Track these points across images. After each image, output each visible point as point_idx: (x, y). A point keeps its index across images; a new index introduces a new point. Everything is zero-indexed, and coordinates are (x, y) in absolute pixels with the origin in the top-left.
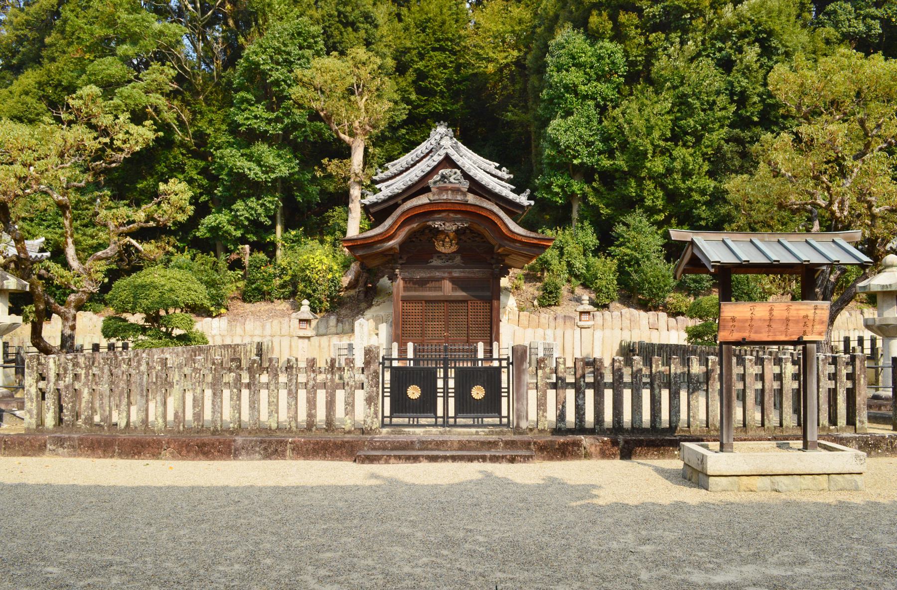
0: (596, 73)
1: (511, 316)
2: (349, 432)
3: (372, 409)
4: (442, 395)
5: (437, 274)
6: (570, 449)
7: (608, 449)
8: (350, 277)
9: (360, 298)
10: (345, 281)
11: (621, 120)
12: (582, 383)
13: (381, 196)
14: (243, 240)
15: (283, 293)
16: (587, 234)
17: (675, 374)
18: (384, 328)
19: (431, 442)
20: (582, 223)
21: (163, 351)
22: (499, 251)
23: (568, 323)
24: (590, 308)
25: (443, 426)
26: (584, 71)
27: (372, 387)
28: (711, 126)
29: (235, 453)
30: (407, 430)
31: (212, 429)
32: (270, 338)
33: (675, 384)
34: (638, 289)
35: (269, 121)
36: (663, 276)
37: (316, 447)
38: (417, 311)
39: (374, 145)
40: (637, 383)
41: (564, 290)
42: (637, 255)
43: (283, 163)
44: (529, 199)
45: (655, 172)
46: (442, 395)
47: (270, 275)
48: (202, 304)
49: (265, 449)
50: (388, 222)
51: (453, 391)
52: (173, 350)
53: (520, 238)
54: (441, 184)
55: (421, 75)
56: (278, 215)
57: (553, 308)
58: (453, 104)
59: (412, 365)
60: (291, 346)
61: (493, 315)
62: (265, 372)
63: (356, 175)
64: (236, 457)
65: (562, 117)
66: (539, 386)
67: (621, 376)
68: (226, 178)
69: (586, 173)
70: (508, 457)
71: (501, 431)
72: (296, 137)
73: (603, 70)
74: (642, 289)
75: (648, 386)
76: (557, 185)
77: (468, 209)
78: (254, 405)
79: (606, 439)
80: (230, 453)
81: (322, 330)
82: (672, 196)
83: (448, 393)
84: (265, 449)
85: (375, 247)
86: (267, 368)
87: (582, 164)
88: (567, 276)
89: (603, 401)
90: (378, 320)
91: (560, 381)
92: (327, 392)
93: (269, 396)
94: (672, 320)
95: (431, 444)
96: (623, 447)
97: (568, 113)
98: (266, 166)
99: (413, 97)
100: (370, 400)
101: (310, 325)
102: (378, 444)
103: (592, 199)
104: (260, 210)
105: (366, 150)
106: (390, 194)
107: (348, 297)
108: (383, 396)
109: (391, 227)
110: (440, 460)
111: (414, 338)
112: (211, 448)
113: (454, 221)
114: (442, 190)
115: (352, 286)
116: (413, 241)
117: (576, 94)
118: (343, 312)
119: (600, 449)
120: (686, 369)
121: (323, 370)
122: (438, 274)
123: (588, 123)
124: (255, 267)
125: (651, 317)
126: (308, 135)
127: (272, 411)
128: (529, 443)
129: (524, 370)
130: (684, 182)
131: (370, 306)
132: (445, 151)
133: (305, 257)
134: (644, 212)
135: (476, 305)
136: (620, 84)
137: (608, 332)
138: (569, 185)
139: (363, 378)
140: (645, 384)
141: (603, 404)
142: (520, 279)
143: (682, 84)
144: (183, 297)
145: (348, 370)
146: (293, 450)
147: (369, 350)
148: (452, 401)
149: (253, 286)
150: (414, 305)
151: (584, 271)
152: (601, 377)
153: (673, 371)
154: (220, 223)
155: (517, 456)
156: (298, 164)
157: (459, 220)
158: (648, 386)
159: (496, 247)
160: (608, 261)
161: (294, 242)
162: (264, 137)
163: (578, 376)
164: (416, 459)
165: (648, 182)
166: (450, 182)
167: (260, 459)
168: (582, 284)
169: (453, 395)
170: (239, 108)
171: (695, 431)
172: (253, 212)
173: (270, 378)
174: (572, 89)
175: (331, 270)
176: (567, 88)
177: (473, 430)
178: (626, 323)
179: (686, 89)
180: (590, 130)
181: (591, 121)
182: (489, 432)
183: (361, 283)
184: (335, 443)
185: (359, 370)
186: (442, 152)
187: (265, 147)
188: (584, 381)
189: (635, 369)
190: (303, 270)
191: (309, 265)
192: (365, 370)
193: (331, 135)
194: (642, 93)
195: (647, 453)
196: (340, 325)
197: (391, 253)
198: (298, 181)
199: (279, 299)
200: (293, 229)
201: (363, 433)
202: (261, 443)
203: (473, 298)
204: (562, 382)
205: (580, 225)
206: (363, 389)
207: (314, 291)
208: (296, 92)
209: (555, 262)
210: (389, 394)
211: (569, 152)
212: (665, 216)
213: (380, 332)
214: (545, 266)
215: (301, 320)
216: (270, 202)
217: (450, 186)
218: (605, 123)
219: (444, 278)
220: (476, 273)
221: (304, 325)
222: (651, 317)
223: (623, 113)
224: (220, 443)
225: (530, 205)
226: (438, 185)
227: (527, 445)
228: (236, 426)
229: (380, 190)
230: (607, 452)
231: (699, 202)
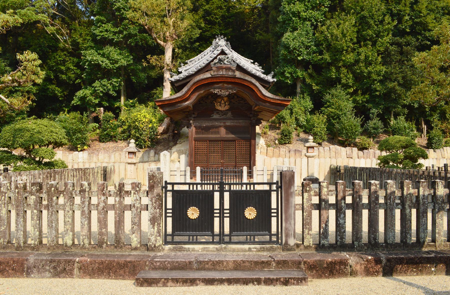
0: (311, 5)
1: (262, 150)
2: (136, 249)
3: (156, 229)
4: (218, 215)
5: (217, 123)
6: (338, 267)
7: (372, 267)
8: (164, 127)
9: (169, 139)
10: (161, 129)
11: (326, 33)
12: (343, 204)
13: (181, 76)
14: (100, 105)
15: (123, 136)
16: (306, 101)
17: (424, 196)
18: (183, 158)
19: (207, 263)
20: (303, 95)
21: (19, 174)
22: (256, 108)
23: (297, 154)
24: (314, 144)
25: (219, 243)
26: (304, 4)
27: (155, 208)
28: (382, 34)
29: (27, 271)
30: (187, 246)
31: (16, 245)
32: (113, 164)
33: (423, 204)
34: (339, 134)
35: (115, 33)
36: (355, 126)
37: (101, 266)
39: (179, 48)
40: (390, 204)
41: (294, 135)
42: (338, 112)
43: (123, 58)
44: (273, 78)
45: (348, 62)
47: (115, 125)
48: (61, 142)
49: (54, 268)
50: (185, 90)
52: (30, 173)
53: (269, 100)
54: (219, 65)
55: (207, 13)
56: (122, 91)
57: (287, 145)
58: (226, 30)
60: (125, 169)
61: (252, 149)
62: (62, 195)
63: (168, 65)
64: (28, 275)
65: (291, 32)
66: (305, 207)
67: (377, 198)
68: (87, 67)
69: (305, 65)
70: (282, 280)
71: (272, 248)
72: (131, 43)
73: (316, 3)
74: (342, 133)
75: (399, 206)
76: (288, 72)
77: (236, 81)
78: (53, 224)
79: (370, 258)
80: (23, 271)
81: (146, 159)
82: (358, 78)
83: (224, 213)
84: (54, 268)
85: (177, 106)
86: (63, 191)
87: (303, 60)
88: (295, 126)
89: (362, 220)
90: (180, 153)
91: (323, 203)
92: (116, 213)
93: (65, 216)
94: (361, 153)
95: (208, 264)
96: (386, 265)
97: (295, 29)
98: (113, 60)
99: (203, 25)
100: (153, 221)
101: (135, 155)
102: (158, 264)
103: (308, 81)
104: (110, 87)
105: (173, 50)
106: (187, 75)
107: (163, 139)
108: (166, 217)
109: (187, 92)
110: (216, 283)
111: (202, 164)
112: (6, 266)
113: (227, 89)
114: (219, 69)
115: (164, 132)
116: (201, 103)
117: (300, 18)
118: (159, 148)
119: (365, 267)
120: (432, 191)
121: (112, 193)
122: (217, 124)
123: (307, 35)
124: (106, 120)
125: (348, 150)
126: (138, 42)
127: (68, 230)
128: (300, 263)
129: (291, 193)
130: (367, 68)
131: (175, 144)
132: (221, 48)
133: (135, 114)
134: (342, 87)
135: (241, 143)
136: (325, 12)
137: (322, 160)
138: (295, 72)
139: (145, 201)
140: (397, 204)
141: (362, 223)
142: (267, 128)
143: (362, 10)
144: (46, 137)
145: (134, 194)
146: (80, 269)
147: (153, 175)
149: (105, 133)
150: (202, 143)
151: (305, 123)
152: (360, 199)
153: (421, 193)
154: (85, 94)
155: (291, 278)
156: (132, 59)
157: (230, 89)
158: (399, 206)
159: (253, 107)
160: (321, 116)
161: (131, 107)
162: (111, 42)
163: (339, 198)
164: (192, 282)
165: (343, 69)
166: (225, 64)
167: (50, 277)
168: (304, 131)
170: (96, 26)
171: (440, 245)
172: (105, 88)
173: (66, 200)
174: (297, 14)
175: (151, 122)
176: (294, 14)
177: (246, 247)
178: (333, 154)
179: (365, 13)
180: (308, 39)
181: (308, 34)
182: (261, 248)
183: (170, 131)
184: (118, 263)
185: (144, 194)
186: (220, 49)
187: (111, 49)
189: (389, 191)
190: (134, 122)
191: (138, 119)
192: (149, 194)
193: (153, 42)
194: (339, 16)
195: (407, 270)
196: (157, 155)
197: (188, 110)
198: (133, 70)
199: (121, 140)
200: (131, 99)
201: (148, 250)
202: (51, 262)
203: (239, 139)
204: (325, 204)
205: (302, 96)
206: (147, 210)
207: (141, 135)
208: (130, 14)
209: (288, 117)
210: (171, 215)
211: (296, 52)
212: (354, 90)
213: (181, 160)
214: (282, 120)
215: (129, 153)
216: (115, 82)
217: (224, 66)
218: (317, 35)
219: (220, 126)
220: (241, 123)
221: (131, 156)
222: (348, 150)
223: (328, 29)
224: (14, 261)
225: (274, 81)
226: (217, 65)
227: (297, 264)
228: (36, 243)
229: (181, 72)
230: (371, 270)
231: (376, 80)
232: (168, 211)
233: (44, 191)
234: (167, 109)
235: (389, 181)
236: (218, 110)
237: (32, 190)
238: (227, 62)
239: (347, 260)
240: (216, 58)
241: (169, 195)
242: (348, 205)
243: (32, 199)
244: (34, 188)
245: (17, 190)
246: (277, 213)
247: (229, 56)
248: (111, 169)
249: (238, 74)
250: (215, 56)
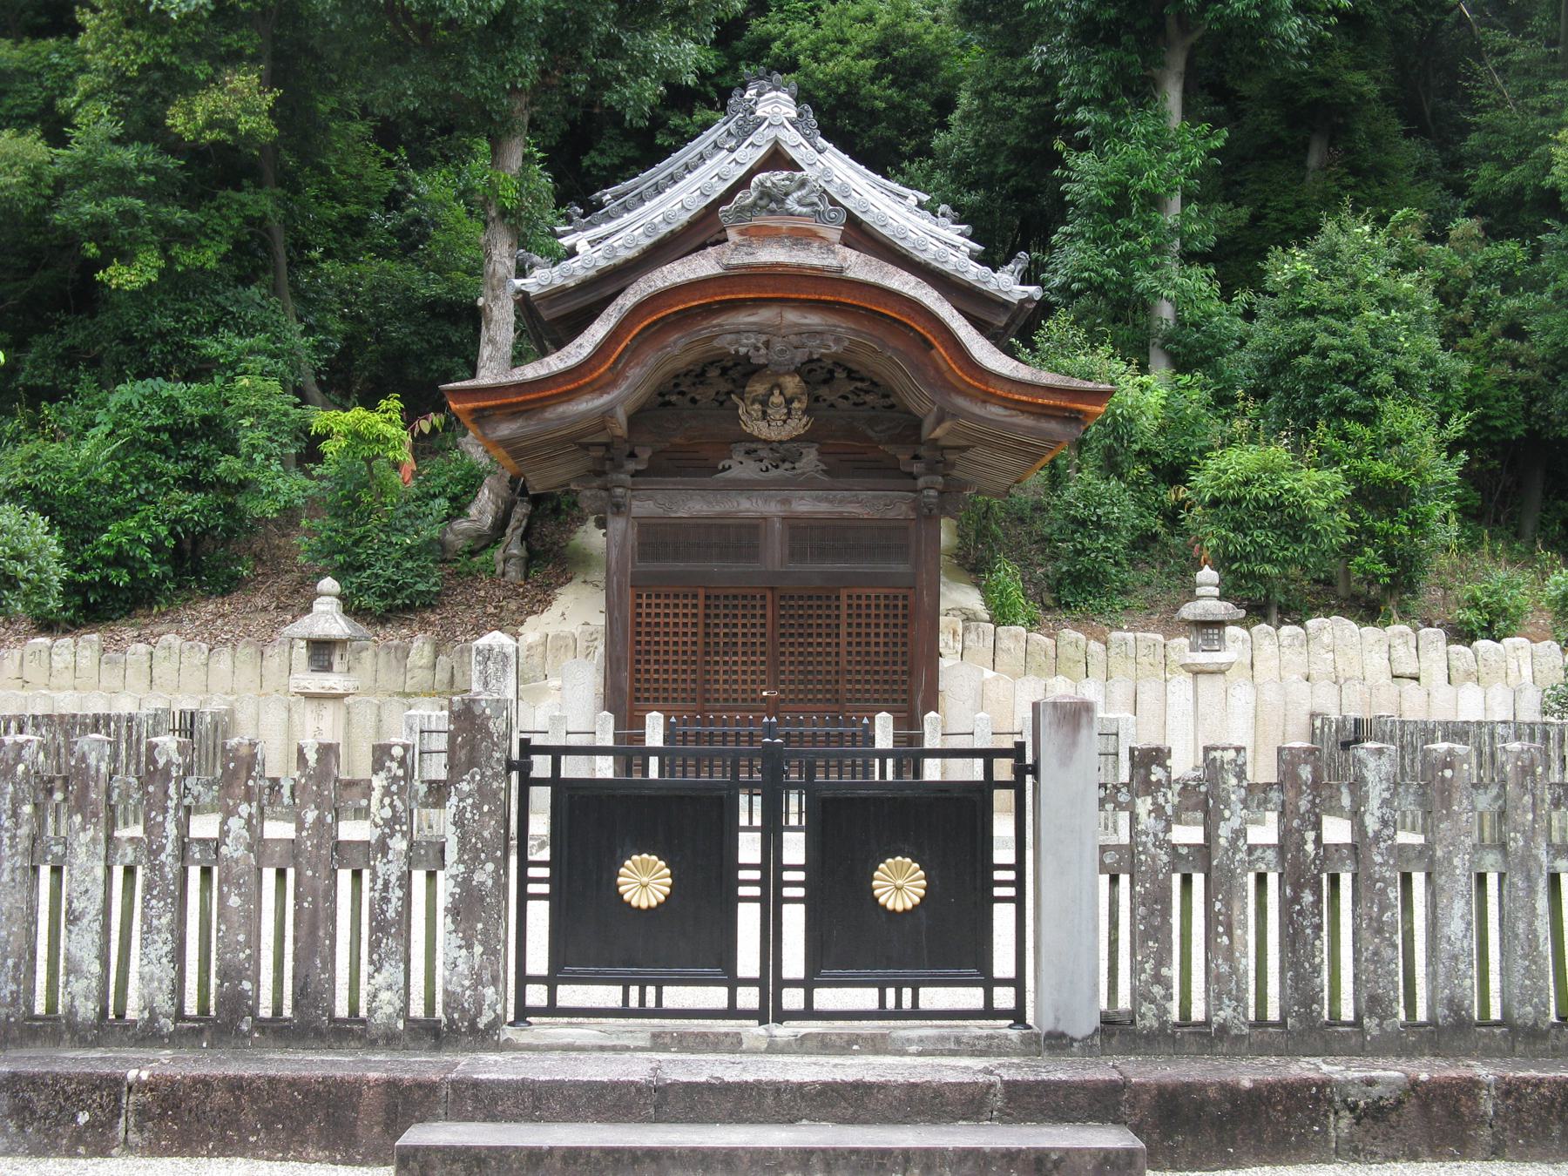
22: (938, 432)
38: (681, 620)
46: (756, 891)
50: (598, 331)
51: (800, 876)
59: (654, 773)
83: (780, 884)
106: (603, 264)
108: (523, 897)
116: (669, 403)
132: (771, 133)
148: (794, 919)
169: (800, 892)
188: (1318, 840)
197: (602, 438)
225: (1030, 299)
229: (572, 253)
232: (533, 872)
234: (506, 429)
236: (752, 438)
238: (800, 202)
240: (743, 183)
241: (541, 798)
246: (1019, 883)
247: (809, 173)
249: (859, 266)
250: (742, 171)
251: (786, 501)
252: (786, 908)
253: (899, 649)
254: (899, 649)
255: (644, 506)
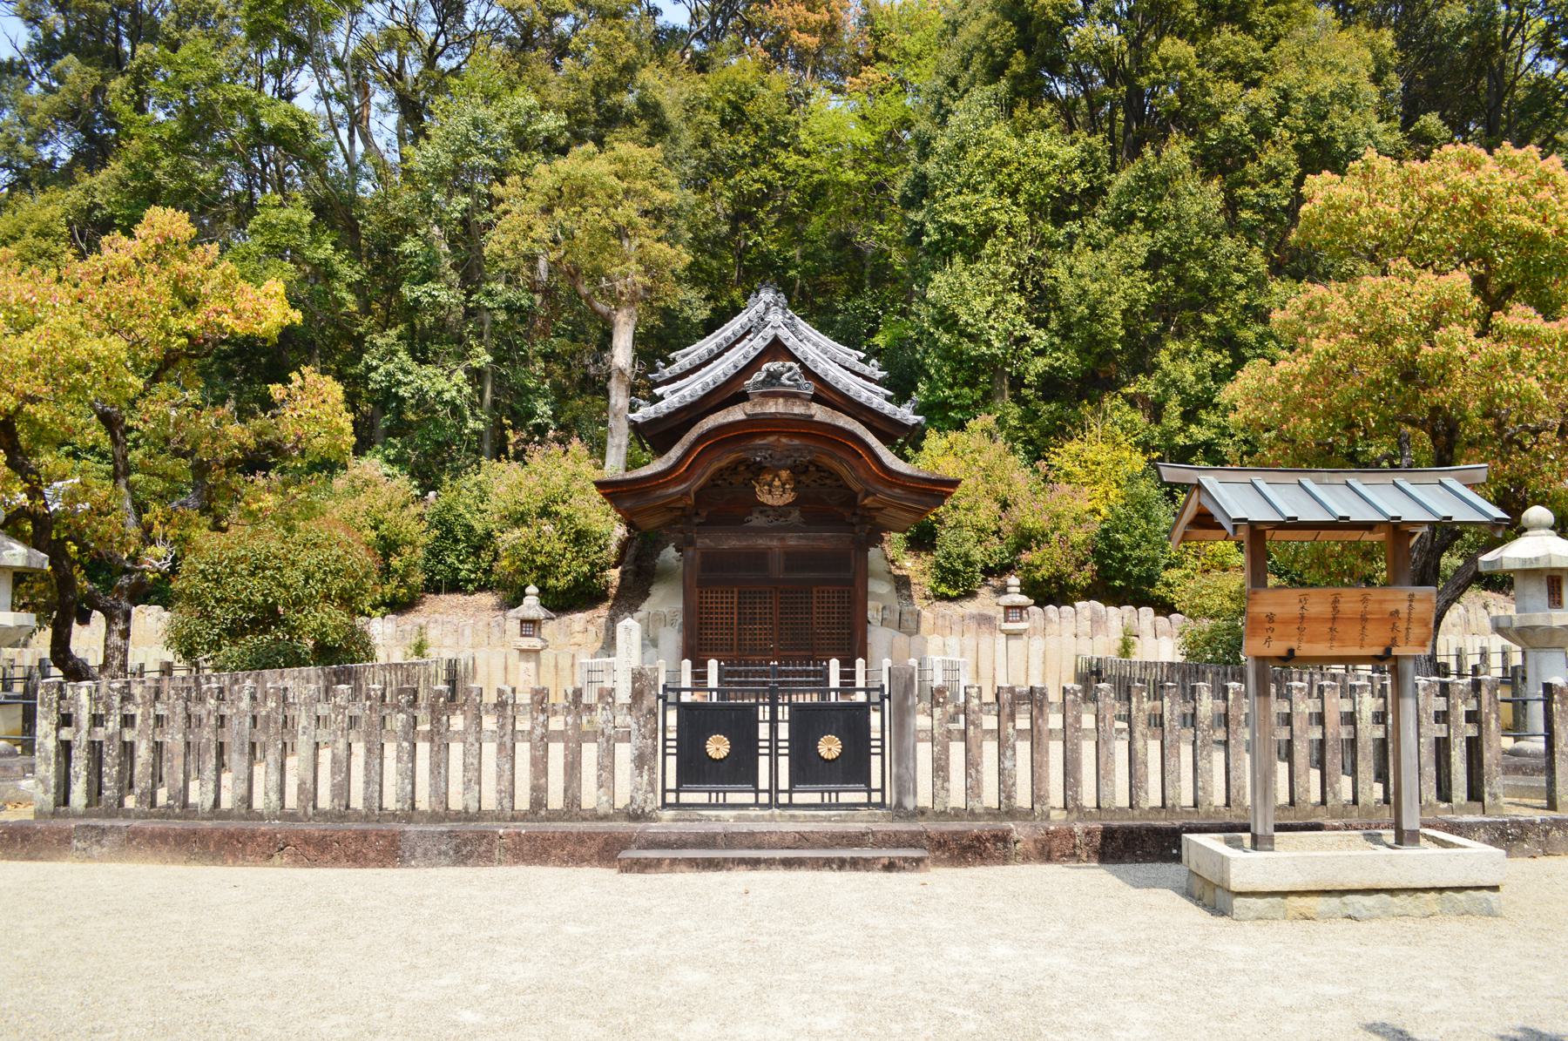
3: (646, 777)
12: (1010, 730)
27: (644, 737)
33: (1171, 731)
83: (777, 748)
89: (1047, 762)
92: (566, 748)
93: (465, 754)
94: (1162, 621)
100: (641, 761)
108: (665, 755)
127: (470, 781)
139: (624, 720)
140: (1120, 731)
148: (784, 763)
159: (860, 497)
173: (467, 722)
178: (1086, 626)
186: (769, 333)
210: (674, 751)
232: (668, 743)
233: (423, 705)
235: (1101, 685)
237: (399, 701)
238: (789, 379)
239: (1010, 831)
242: (1020, 732)
243: (398, 721)
244: (403, 699)
245: (368, 703)
246: (883, 747)
248: (467, 665)
249: (819, 413)
251: (782, 539)
252: (780, 758)
253: (846, 621)
254: (846, 621)
255: (704, 542)
